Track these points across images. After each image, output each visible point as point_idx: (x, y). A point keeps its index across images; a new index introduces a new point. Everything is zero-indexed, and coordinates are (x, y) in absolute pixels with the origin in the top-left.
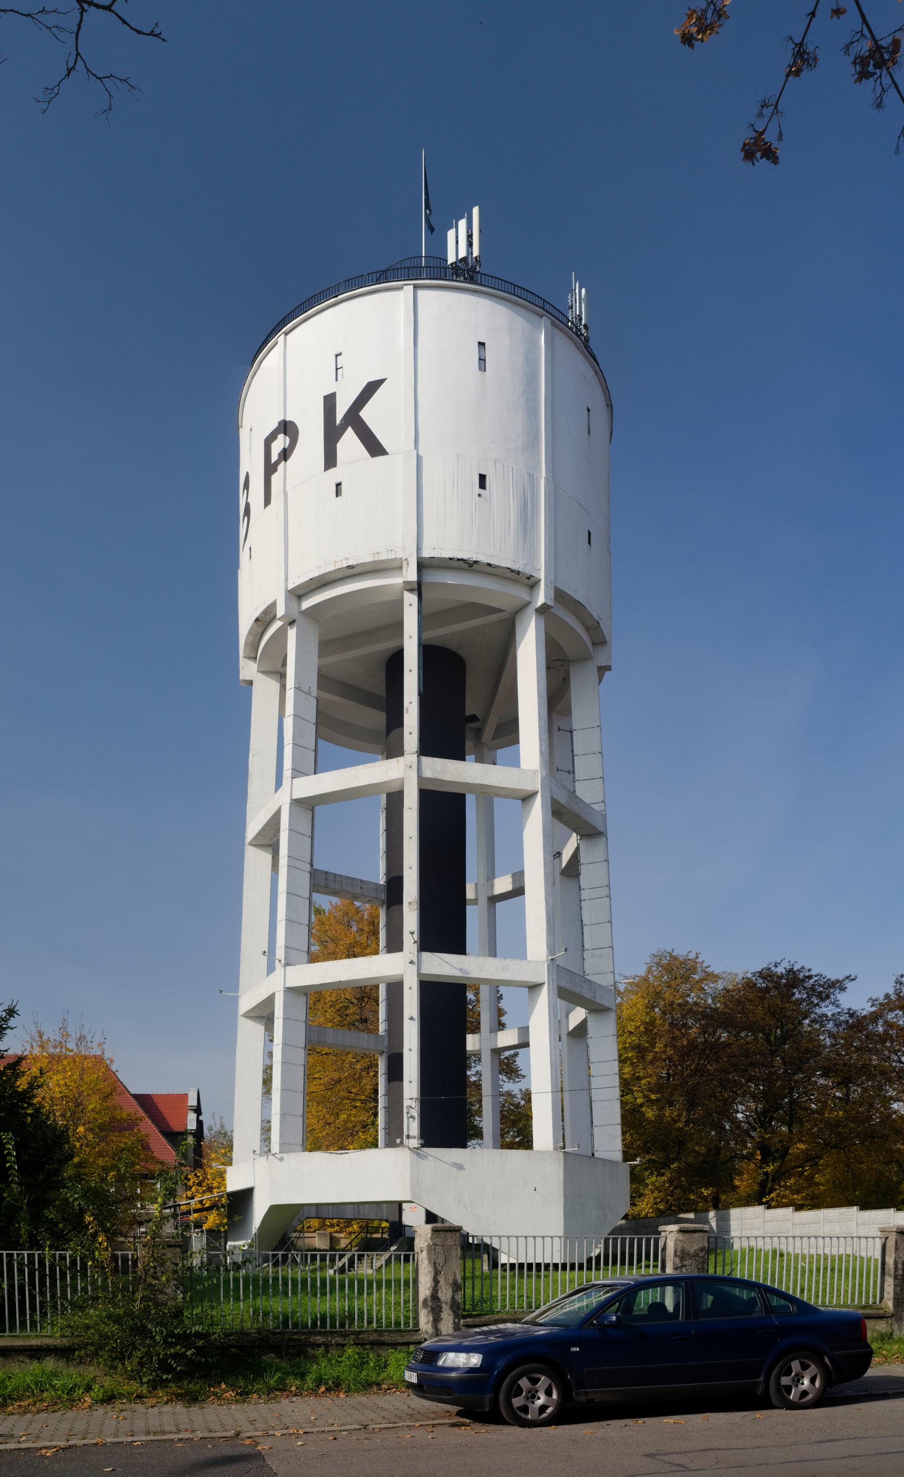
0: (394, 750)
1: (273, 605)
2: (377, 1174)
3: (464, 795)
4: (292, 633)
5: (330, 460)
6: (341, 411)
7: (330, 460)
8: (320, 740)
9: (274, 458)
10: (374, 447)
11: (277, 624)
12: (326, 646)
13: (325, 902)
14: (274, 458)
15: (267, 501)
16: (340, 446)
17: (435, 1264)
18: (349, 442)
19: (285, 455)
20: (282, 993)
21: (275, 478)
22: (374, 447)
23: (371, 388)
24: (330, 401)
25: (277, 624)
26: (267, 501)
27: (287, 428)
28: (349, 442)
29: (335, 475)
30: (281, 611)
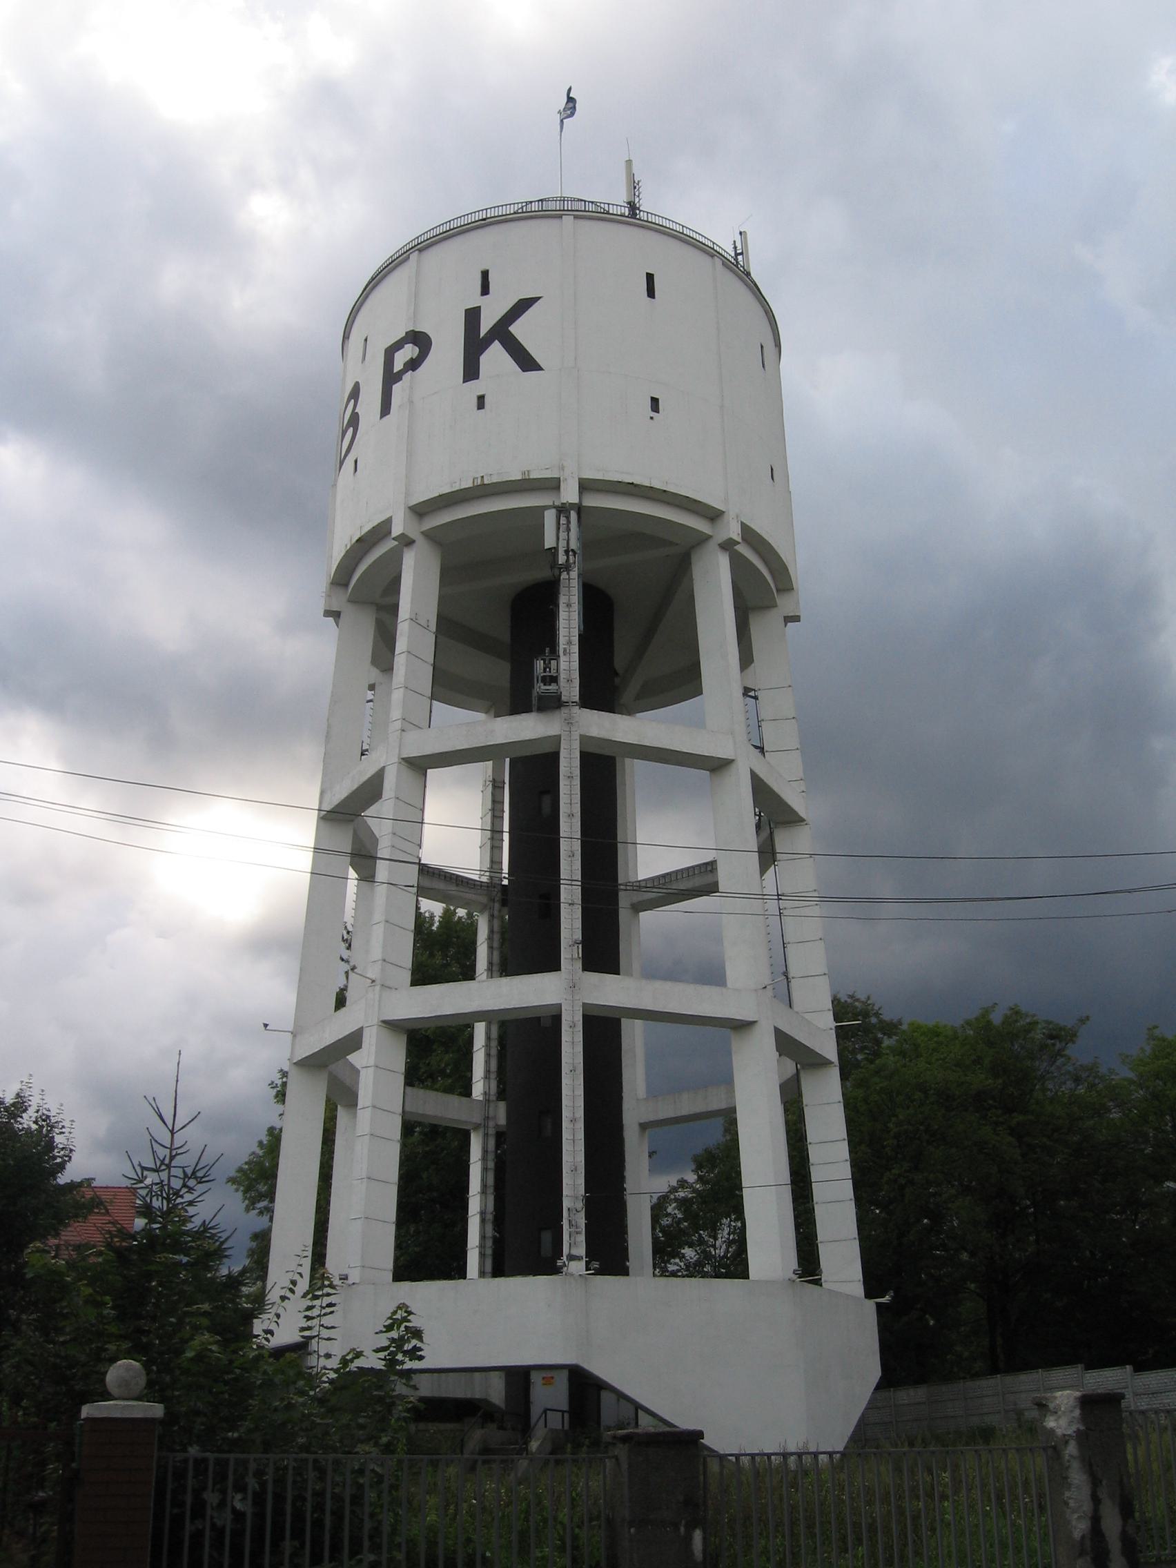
0: (550, 963)
1: (388, 522)
2: (486, 1324)
3: (619, 1020)
4: (409, 561)
5: (471, 371)
6: (485, 327)
7: (471, 371)
8: (435, 702)
9: (398, 366)
10: (526, 362)
11: (388, 545)
12: (448, 575)
13: (433, 908)
14: (398, 366)
15: (386, 409)
16: (484, 359)
17: (1091, 1465)
18: (495, 358)
19: (413, 365)
20: (374, 1029)
21: (396, 388)
22: (526, 362)
23: (524, 305)
24: (473, 316)
25: (388, 545)
26: (386, 409)
27: (420, 340)
28: (495, 358)
29: (476, 388)
30: (397, 530)
